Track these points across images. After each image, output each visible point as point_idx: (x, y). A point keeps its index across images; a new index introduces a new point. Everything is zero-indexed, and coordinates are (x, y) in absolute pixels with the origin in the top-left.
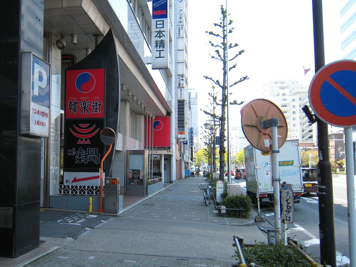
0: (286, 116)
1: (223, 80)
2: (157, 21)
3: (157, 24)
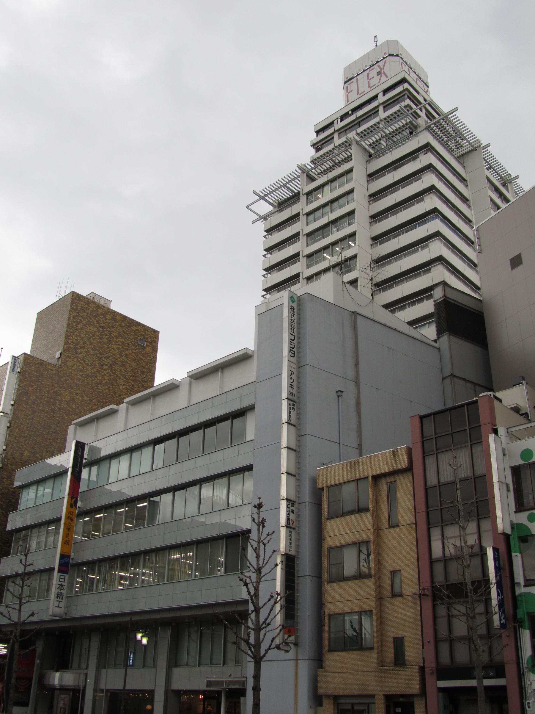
0: (71, 290)
1: (456, 288)
2: (60, 576)
3: (64, 579)
